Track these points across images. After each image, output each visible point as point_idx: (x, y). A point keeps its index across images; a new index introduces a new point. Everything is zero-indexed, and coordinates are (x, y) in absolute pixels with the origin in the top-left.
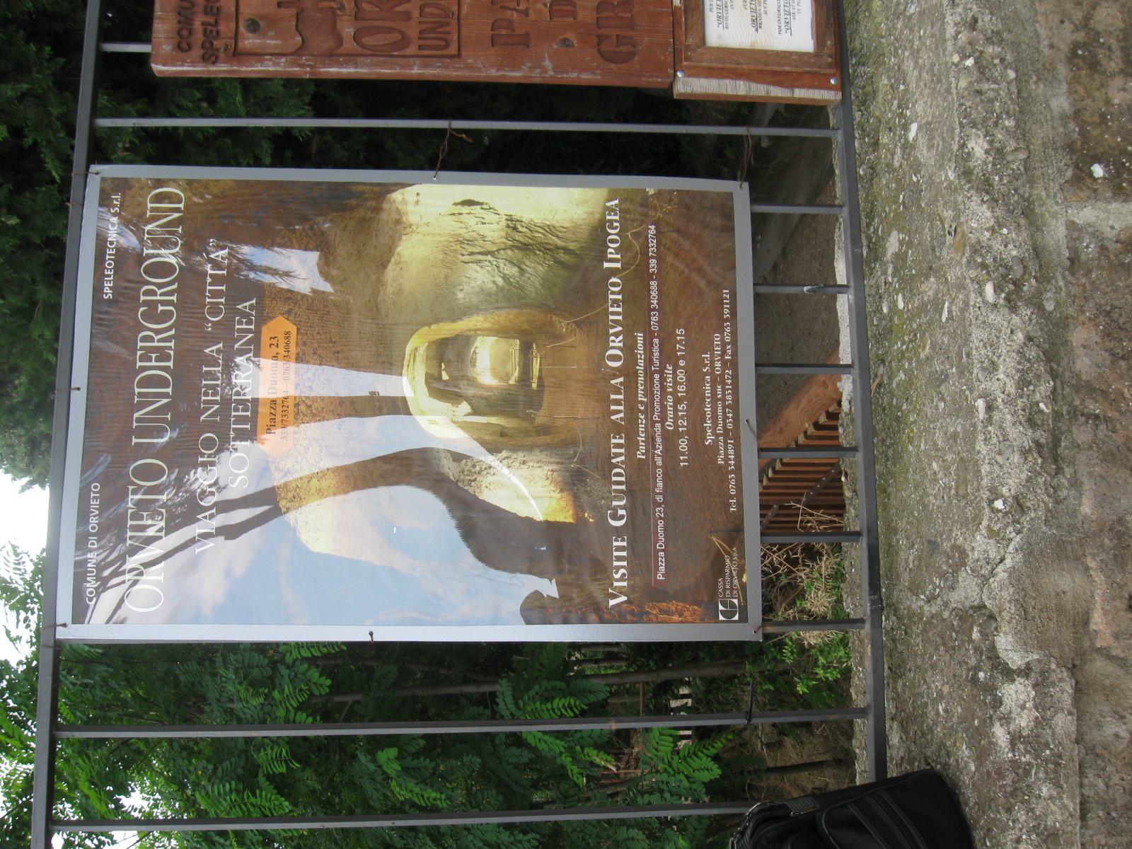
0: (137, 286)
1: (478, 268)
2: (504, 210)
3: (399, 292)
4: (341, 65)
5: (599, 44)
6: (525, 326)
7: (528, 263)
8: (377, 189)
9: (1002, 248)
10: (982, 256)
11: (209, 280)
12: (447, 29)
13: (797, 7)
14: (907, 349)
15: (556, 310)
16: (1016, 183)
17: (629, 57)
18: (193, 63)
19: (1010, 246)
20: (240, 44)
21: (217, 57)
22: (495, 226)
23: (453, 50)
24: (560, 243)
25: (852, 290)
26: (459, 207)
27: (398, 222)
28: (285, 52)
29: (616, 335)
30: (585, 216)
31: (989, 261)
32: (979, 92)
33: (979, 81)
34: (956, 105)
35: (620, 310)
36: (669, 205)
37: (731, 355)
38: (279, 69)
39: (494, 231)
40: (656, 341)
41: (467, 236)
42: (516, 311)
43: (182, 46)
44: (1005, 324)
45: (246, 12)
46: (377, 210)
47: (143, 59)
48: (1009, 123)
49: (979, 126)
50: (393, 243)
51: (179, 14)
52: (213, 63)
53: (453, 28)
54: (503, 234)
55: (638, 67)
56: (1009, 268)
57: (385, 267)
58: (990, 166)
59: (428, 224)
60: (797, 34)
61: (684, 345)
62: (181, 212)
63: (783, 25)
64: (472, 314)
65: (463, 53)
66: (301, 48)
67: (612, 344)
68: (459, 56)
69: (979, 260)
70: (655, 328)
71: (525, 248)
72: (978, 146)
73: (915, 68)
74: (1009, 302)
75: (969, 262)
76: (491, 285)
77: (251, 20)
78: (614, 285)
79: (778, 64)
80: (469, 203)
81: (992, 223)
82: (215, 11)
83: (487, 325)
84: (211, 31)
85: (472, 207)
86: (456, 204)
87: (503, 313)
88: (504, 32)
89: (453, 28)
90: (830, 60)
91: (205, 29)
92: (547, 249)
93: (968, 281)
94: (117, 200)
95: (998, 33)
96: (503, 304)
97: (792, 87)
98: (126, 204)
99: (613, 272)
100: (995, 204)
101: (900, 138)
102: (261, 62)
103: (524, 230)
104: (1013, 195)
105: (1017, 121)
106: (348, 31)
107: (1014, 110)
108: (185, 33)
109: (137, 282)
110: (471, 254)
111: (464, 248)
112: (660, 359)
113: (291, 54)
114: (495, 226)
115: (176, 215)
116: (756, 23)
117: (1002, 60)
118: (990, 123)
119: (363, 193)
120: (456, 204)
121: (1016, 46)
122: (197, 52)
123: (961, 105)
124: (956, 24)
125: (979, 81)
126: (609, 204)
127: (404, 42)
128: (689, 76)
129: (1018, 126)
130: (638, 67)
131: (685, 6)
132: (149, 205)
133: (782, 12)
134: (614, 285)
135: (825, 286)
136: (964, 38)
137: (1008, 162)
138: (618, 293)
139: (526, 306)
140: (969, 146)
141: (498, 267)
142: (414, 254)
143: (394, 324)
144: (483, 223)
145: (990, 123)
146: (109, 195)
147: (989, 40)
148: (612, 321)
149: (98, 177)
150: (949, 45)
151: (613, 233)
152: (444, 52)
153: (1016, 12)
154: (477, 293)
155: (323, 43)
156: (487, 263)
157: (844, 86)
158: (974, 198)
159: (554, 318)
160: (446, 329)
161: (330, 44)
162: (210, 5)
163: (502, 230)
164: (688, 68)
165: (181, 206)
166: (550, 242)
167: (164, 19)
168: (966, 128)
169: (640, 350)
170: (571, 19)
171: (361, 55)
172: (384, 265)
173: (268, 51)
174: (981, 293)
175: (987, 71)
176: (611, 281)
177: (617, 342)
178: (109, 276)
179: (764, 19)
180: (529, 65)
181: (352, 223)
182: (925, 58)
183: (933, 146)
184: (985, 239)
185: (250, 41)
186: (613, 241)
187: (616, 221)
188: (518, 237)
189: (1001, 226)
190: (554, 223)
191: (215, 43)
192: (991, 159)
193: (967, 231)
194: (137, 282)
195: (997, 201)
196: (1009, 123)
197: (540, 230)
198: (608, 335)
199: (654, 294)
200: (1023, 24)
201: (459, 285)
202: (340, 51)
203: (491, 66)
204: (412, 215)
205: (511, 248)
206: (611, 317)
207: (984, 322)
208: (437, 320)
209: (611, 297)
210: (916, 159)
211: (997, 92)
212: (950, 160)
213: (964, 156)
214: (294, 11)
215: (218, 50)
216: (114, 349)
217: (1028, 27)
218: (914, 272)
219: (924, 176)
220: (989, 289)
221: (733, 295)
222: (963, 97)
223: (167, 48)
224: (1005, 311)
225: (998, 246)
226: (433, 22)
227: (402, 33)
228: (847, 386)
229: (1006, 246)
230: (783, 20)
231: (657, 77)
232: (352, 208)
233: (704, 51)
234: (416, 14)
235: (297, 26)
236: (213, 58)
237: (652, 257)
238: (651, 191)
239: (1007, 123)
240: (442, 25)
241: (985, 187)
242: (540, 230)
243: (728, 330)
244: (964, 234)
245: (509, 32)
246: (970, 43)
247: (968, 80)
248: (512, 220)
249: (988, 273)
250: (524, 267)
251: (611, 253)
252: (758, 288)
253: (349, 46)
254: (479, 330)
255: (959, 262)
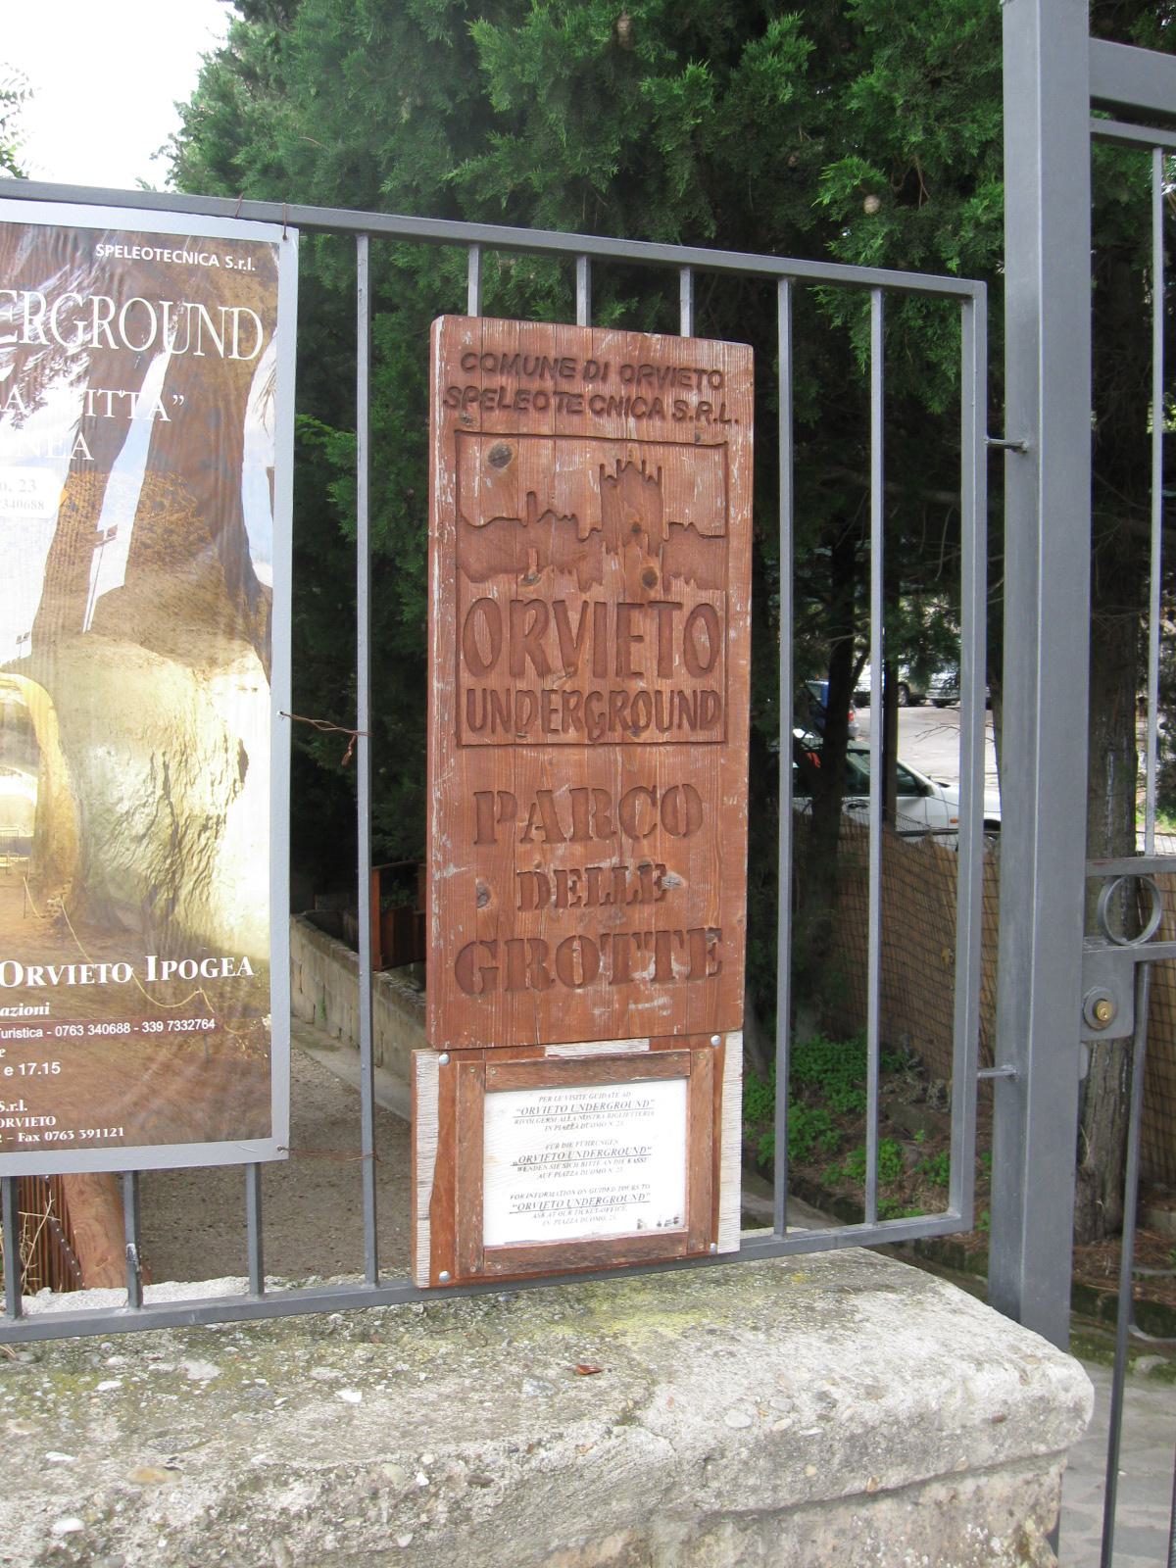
0: (115, 293)
1: (143, 776)
2: (233, 813)
3: (105, 664)
4: (443, 580)
5: (482, 942)
6: (54, 845)
7: (152, 847)
8: (263, 630)
9: (137, 1541)
10: (126, 1510)
11: (122, 394)
12: (499, 728)
13: (552, 1220)
14: (34, 1398)
15: (80, 889)
16: (238, 1555)
17: (465, 986)
18: (445, 374)
19: (139, 1552)
20: (473, 439)
21: (454, 407)
22: (208, 799)
23: (468, 737)
24: (184, 893)
25: (132, 1312)
26: (237, 748)
27: (213, 662)
28: (462, 502)
29: (46, 976)
30: (227, 928)
31: (116, 1522)
32: (375, 1495)
33: (392, 1493)
34: (357, 1463)
35: (84, 980)
36: (248, 1048)
37: (24, 1142)
38: (437, 493)
39: (199, 798)
40: (40, 1033)
41: (192, 760)
42: (77, 831)
43: (471, 360)
44: (18, 1551)
45: (520, 448)
46: (231, 632)
47: (458, 309)
48: (330, 1542)
49: (324, 1498)
50: (181, 655)
51: (517, 355)
52: (445, 402)
53: (501, 736)
54: (197, 811)
55: (451, 998)
56: (105, 1551)
57: (142, 644)
58: (263, 1516)
59: (210, 704)
60: (509, 1221)
61: (35, 1071)
62: (226, 355)
63: (525, 1201)
64: (72, 769)
65: (464, 752)
66: (468, 524)
67: (30, 970)
68: (459, 745)
69: (119, 1507)
70: (59, 1031)
71: (175, 842)
72: (295, 1497)
73: (440, 1395)
74: (53, 1555)
75: (118, 1491)
76: (116, 795)
77: (510, 454)
78: (122, 971)
79: (462, 1197)
80: (243, 761)
81: (175, 1523)
82: (522, 405)
83: (55, 790)
84: (492, 399)
85: (237, 767)
86: (241, 744)
87: (75, 813)
88: (496, 808)
89: (501, 736)
90: (473, 1270)
91: (495, 392)
92: (172, 877)
93: (88, 1491)
94: (245, 265)
95: (468, 1518)
96: (87, 813)
97: (432, 1216)
98: (239, 277)
99: (141, 970)
100: (203, 1526)
101: (348, 1376)
102: (447, 469)
103: (203, 841)
104: (219, 1552)
105: (334, 1552)
106: (494, 590)
107: (352, 1547)
108: (489, 363)
109: (120, 293)
110: (166, 767)
111: (175, 759)
112: (11, 1040)
113: (458, 510)
114: (208, 799)
115: (221, 348)
116: (525, 1163)
117: (427, 1526)
118: (329, 1513)
119: (257, 612)
120: (241, 744)
121: (451, 1543)
122: (462, 379)
123: (357, 1470)
124: (479, 1457)
125: (392, 1493)
126: (245, 961)
127: (478, 668)
128: (442, 1070)
129: (325, 1553)
130: (451, 998)
131: (544, 1063)
132: (236, 311)
133: (544, 1199)
134: (122, 971)
135: (137, 1274)
136: (457, 1470)
137: (269, 1543)
138: (109, 978)
139: (85, 846)
140: (296, 1484)
141: (144, 805)
142: (162, 685)
143: (56, 659)
144: (212, 784)
145: (329, 1513)
146: (253, 255)
147: (455, 1505)
148: (66, 970)
149: (279, 240)
150: (451, 1448)
151: (200, 969)
152: (465, 726)
153: (503, 1540)
154: (104, 776)
155: (477, 554)
156: (151, 789)
157: (436, 1288)
158: (215, 1495)
159: (68, 887)
160: (48, 732)
161: (475, 564)
162: (531, 398)
163: (203, 811)
164: (454, 1069)
165: (235, 355)
166: (185, 878)
167: (510, 333)
168: (322, 1479)
169: (24, 1011)
170: (518, 903)
171: (458, 608)
172: (145, 642)
173: (463, 478)
174: (67, 1512)
175: (410, 1505)
176: (127, 966)
177: (35, 978)
178: (130, 253)
179: (531, 1175)
180: (449, 845)
181: (209, 597)
182: (450, 1409)
183: (314, 1428)
184: (150, 1515)
185: (477, 453)
186: (188, 970)
187: (220, 972)
188: (192, 832)
189: (171, 1537)
190: (215, 884)
191: (475, 405)
192: (273, 1517)
193: (163, 1488)
194: (120, 293)
195: (208, 1528)
196: (330, 1542)
197: (203, 864)
198: (44, 964)
199: (111, 1029)
200: (485, 1552)
201: (117, 749)
202: (464, 579)
203: (444, 793)
204: (222, 681)
205: (175, 824)
206: (72, 968)
207: (22, 1519)
208: (62, 720)
209: (103, 967)
210: (307, 1401)
211: (377, 1521)
212: (281, 1456)
213: (281, 1478)
214: (523, 514)
215: (465, 408)
216: (21, 257)
217: (482, 1559)
218: (143, 1404)
219: (276, 1415)
220: (73, 1524)
221: (120, 1142)
222: (368, 1472)
223: (467, 338)
224: (38, 1549)
225: (139, 1534)
226: (509, 712)
227: (491, 666)
228: (106, 1299)
229: (139, 1545)
230: (531, 1200)
231: (438, 1025)
232: (232, 596)
233: (477, 1092)
234: (522, 685)
235: (503, 518)
236: (452, 402)
237: (166, 1026)
238: (267, 1021)
239: (330, 1537)
240: (506, 723)
241: (231, 1512)
242: (203, 864)
243: (63, 1136)
244: (161, 1482)
245: (497, 816)
246: (449, 1479)
247: (395, 1480)
248: (218, 824)
249: (98, 1521)
250: (145, 842)
251: (170, 966)
252: (130, 1177)
253: (473, 591)
254: (48, 778)
255: (122, 1477)
